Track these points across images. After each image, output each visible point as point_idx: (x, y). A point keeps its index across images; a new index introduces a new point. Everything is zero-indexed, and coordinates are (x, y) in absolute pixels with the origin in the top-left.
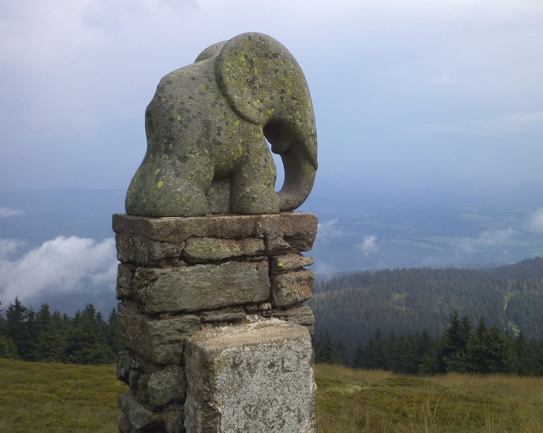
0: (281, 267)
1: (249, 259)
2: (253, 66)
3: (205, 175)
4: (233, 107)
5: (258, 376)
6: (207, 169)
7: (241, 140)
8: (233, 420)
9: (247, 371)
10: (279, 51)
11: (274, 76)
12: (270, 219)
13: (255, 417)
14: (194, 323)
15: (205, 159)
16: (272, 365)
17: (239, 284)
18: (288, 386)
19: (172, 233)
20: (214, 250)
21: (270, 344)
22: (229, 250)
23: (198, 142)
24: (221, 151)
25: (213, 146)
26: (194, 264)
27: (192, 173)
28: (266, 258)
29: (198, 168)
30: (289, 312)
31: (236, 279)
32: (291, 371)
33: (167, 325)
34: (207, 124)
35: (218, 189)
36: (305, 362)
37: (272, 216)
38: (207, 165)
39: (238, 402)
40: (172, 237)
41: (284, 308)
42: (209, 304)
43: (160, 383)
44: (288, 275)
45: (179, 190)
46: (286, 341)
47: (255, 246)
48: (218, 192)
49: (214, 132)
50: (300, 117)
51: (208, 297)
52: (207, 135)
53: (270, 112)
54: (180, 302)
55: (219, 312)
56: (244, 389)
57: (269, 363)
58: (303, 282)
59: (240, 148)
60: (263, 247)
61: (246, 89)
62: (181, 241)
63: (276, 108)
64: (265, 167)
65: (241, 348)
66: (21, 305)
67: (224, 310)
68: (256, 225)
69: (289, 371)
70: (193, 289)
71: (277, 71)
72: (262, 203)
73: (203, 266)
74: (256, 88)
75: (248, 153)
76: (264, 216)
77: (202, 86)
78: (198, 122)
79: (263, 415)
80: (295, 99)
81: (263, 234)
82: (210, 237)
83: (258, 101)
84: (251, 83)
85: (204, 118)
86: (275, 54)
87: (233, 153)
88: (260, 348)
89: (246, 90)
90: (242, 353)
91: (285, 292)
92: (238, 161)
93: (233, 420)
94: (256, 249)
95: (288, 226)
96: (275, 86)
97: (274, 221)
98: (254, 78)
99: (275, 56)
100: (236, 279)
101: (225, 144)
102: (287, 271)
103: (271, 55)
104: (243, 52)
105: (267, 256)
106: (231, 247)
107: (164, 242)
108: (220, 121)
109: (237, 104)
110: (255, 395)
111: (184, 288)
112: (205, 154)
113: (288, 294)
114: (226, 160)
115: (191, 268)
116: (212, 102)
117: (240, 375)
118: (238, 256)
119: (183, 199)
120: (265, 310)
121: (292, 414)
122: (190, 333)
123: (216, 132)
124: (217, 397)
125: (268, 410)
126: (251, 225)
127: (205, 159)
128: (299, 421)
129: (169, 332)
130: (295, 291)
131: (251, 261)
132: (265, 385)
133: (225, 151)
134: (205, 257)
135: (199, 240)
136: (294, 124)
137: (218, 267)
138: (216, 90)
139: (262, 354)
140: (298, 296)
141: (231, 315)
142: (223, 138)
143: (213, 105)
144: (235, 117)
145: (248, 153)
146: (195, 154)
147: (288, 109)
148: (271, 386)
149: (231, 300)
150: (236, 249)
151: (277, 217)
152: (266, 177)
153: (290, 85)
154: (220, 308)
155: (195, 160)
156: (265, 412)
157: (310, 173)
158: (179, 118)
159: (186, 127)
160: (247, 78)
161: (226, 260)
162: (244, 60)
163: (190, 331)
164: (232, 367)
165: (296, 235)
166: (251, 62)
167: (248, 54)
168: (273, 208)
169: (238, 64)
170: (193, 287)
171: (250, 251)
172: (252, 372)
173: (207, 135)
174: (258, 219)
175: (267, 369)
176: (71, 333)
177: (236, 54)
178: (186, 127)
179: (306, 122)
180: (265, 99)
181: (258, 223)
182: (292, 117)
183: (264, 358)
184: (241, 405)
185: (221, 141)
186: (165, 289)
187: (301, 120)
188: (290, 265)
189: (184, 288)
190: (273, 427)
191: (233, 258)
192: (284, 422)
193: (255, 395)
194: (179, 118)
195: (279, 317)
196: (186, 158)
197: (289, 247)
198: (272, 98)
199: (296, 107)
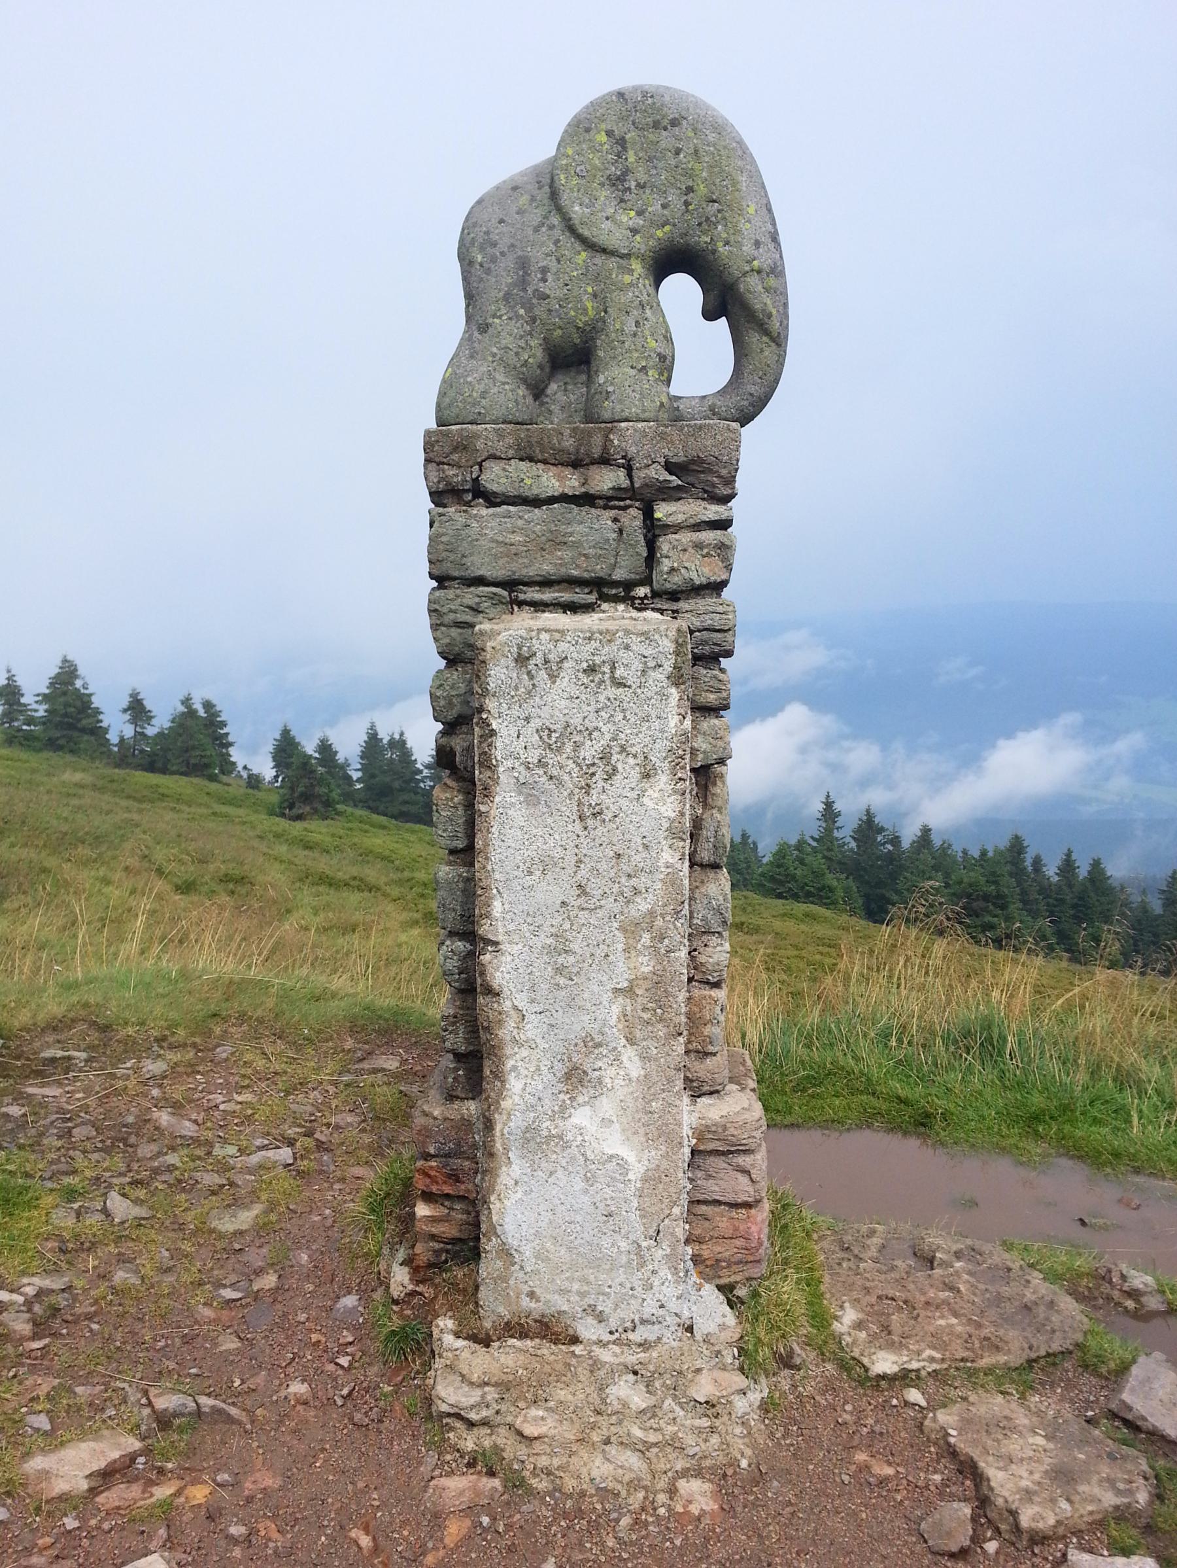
0: (659, 520)
1: (601, 502)
2: (625, 149)
3: (517, 354)
4: (572, 230)
5: (565, 681)
6: (522, 343)
7: (590, 290)
8: (518, 746)
9: (543, 672)
10: (683, 113)
11: (673, 162)
12: (635, 430)
13: (559, 750)
14: (496, 600)
15: (518, 325)
16: (591, 670)
17: (577, 545)
18: (624, 711)
19: (455, 449)
20: (528, 482)
21: (588, 635)
22: (557, 484)
23: (507, 297)
24: (550, 311)
25: (534, 301)
26: (499, 505)
27: (495, 350)
28: (637, 504)
29: (504, 342)
30: (683, 605)
31: (571, 534)
32: (629, 687)
33: (451, 596)
34: (523, 264)
35: (565, 384)
36: (660, 676)
37: (640, 425)
38: (521, 337)
39: (527, 719)
40: (455, 457)
41: (673, 596)
42: (524, 572)
43: (441, 685)
44: (677, 536)
45: (469, 379)
46: (620, 634)
47: (607, 480)
48: (565, 390)
49: (536, 276)
50: (724, 235)
51: (520, 561)
52: (523, 283)
53: (659, 233)
54: (473, 563)
55: (547, 590)
56: (537, 699)
57: (585, 665)
58: (705, 551)
59: (589, 305)
60: (625, 483)
61: (604, 194)
62: (470, 463)
63: (674, 225)
64: (635, 335)
65: (534, 634)
66: (876, 820)
67: (556, 588)
68: (607, 439)
69: (625, 686)
70: (494, 545)
71: (678, 152)
72: (621, 401)
73: (511, 508)
74: (629, 189)
75: (606, 312)
76: (623, 424)
77: (524, 200)
78: (509, 262)
79: (574, 751)
80: (714, 201)
81: (623, 457)
82: (521, 460)
83: (632, 213)
84: (617, 182)
85: (520, 253)
86: (675, 119)
87: (573, 313)
88: (569, 638)
89: (604, 193)
90: (534, 641)
91: (666, 565)
92: (588, 328)
93: (518, 746)
94: (610, 485)
95: (672, 442)
96: (673, 181)
97: (644, 435)
98: (627, 172)
99: (675, 123)
100: (571, 534)
101: (555, 298)
102: (677, 528)
103: (665, 122)
104: (603, 126)
105: (641, 500)
106: (561, 479)
107: (443, 463)
108: (547, 255)
109: (576, 222)
110: (557, 713)
111: (477, 540)
112: (518, 317)
113: (673, 569)
114: (560, 327)
115: (491, 510)
116: (535, 223)
117: (531, 677)
118: (575, 496)
119: (475, 394)
120: (640, 598)
121: (631, 761)
122: (491, 616)
123: (539, 276)
124: (490, 704)
125: (583, 744)
126: (597, 441)
127: (518, 325)
128: (647, 776)
129: (453, 607)
130: (686, 565)
131: (605, 507)
132: (577, 701)
133: (556, 310)
134: (512, 492)
135: (502, 464)
136: (714, 252)
137: (536, 510)
138: (546, 201)
139: (572, 649)
140: (694, 575)
141: (566, 597)
142: (551, 287)
143: (536, 230)
144: (578, 246)
145: (606, 312)
146: (500, 317)
147: (700, 224)
148: (589, 705)
149: (563, 570)
150: (572, 483)
151: (650, 428)
152: (637, 355)
153: (704, 174)
154: (546, 583)
155: (500, 329)
156: (577, 746)
157: (762, 351)
158: (479, 258)
159: (488, 271)
160: (608, 172)
161: (551, 500)
162: (604, 138)
163: (492, 612)
164: (516, 661)
165: (692, 462)
166: (622, 142)
167: (614, 128)
168: (644, 411)
169: (590, 148)
170: (492, 541)
171: (598, 488)
172: (553, 677)
173: (523, 283)
174: (611, 430)
175: (581, 675)
176: (960, 882)
177: (588, 130)
178: (488, 271)
179: (739, 244)
180: (650, 209)
181: (612, 437)
182: (708, 240)
183: (575, 655)
184: (532, 724)
185: (548, 292)
186: (444, 539)
187: (727, 243)
188: (680, 518)
189: (477, 540)
190: (593, 774)
191: (564, 498)
192: (615, 770)
193: (557, 713)
194: (479, 258)
195: (661, 611)
196: (488, 325)
197: (679, 486)
198: (664, 206)
199: (716, 217)
